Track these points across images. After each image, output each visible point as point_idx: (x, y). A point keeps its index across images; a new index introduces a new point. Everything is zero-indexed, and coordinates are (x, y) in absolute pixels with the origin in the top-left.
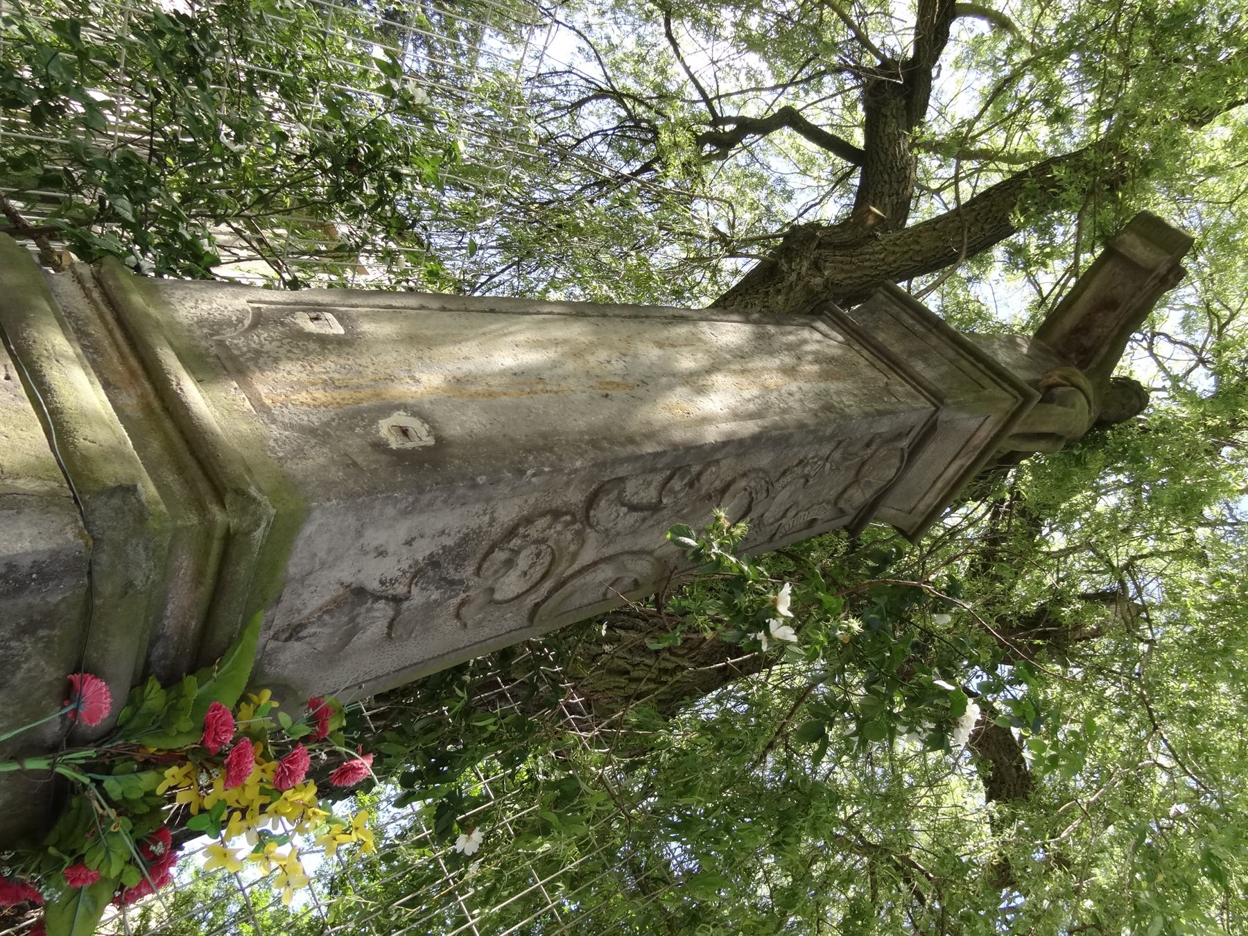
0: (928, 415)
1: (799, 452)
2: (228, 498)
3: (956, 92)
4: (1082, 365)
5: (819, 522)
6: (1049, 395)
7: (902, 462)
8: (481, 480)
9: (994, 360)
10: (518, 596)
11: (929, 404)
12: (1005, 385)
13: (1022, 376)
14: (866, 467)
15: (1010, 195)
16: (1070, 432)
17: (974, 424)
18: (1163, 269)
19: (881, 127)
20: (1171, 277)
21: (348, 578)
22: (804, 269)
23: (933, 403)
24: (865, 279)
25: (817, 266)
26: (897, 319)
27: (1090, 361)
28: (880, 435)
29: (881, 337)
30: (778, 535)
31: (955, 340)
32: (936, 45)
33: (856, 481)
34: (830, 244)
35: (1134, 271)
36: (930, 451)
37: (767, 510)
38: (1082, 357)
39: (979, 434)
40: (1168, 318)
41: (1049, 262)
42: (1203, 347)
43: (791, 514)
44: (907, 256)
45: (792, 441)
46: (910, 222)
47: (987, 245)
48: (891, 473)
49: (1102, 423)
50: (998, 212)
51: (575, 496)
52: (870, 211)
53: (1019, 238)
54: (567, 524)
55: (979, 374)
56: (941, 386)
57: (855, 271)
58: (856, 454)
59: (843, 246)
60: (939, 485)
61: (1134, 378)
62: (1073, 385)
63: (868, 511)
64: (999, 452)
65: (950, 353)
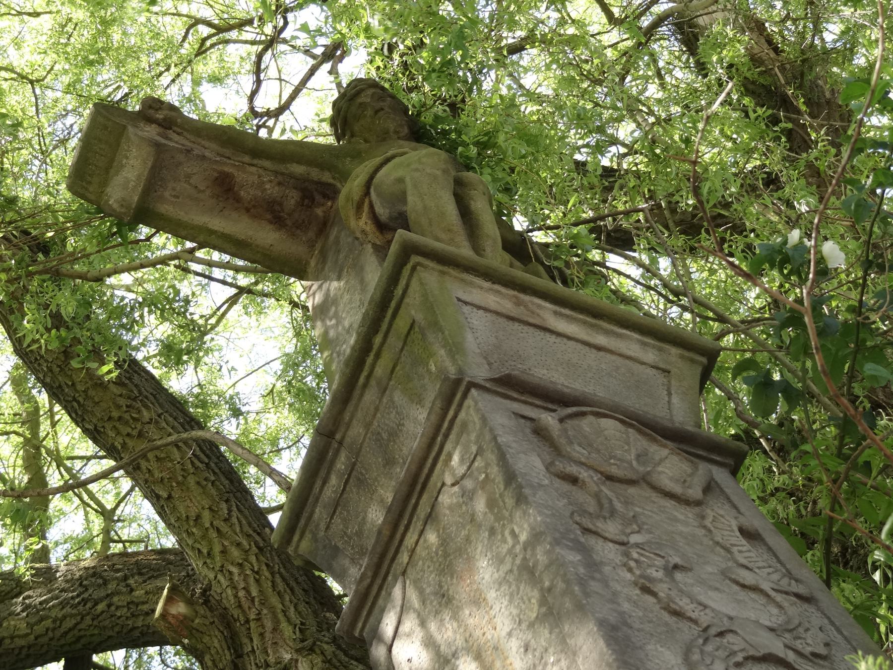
0: (488, 396)
1: (629, 600)
4: (330, 192)
5: (745, 522)
7: (583, 414)
9: (362, 325)
11: (469, 402)
12: (399, 291)
13: (374, 274)
14: (614, 471)
15: (87, 397)
16: (445, 171)
17: (478, 319)
18: (151, 131)
20: (160, 116)
23: (465, 396)
24: (281, 586)
26: (337, 504)
27: (320, 183)
28: (548, 467)
29: (376, 516)
30: (795, 588)
31: (346, 395)
33: (645, 481)
35: (164, 169)
37: (757, 622)
38: (318, 197)
39: (493, 306)
40: (224, 104)
41: (125, 5)
42: (253, 43)
43: (748, 578)
44: (225, 528)
45: (613, 619)
46: (169, 542)
47: (175, 405)
48: (609, 425)
49: (418, 133)
50: (119, 407)
52: (163, 615)
53: (147, 355)
55: (391, 339)
56: (432, 392)
58: (597, 496)
60: (601, 340)
61: (329, 112)
62: (367, 193)
63: (688, 442)
64: (511, 266)
65: (370, 396)
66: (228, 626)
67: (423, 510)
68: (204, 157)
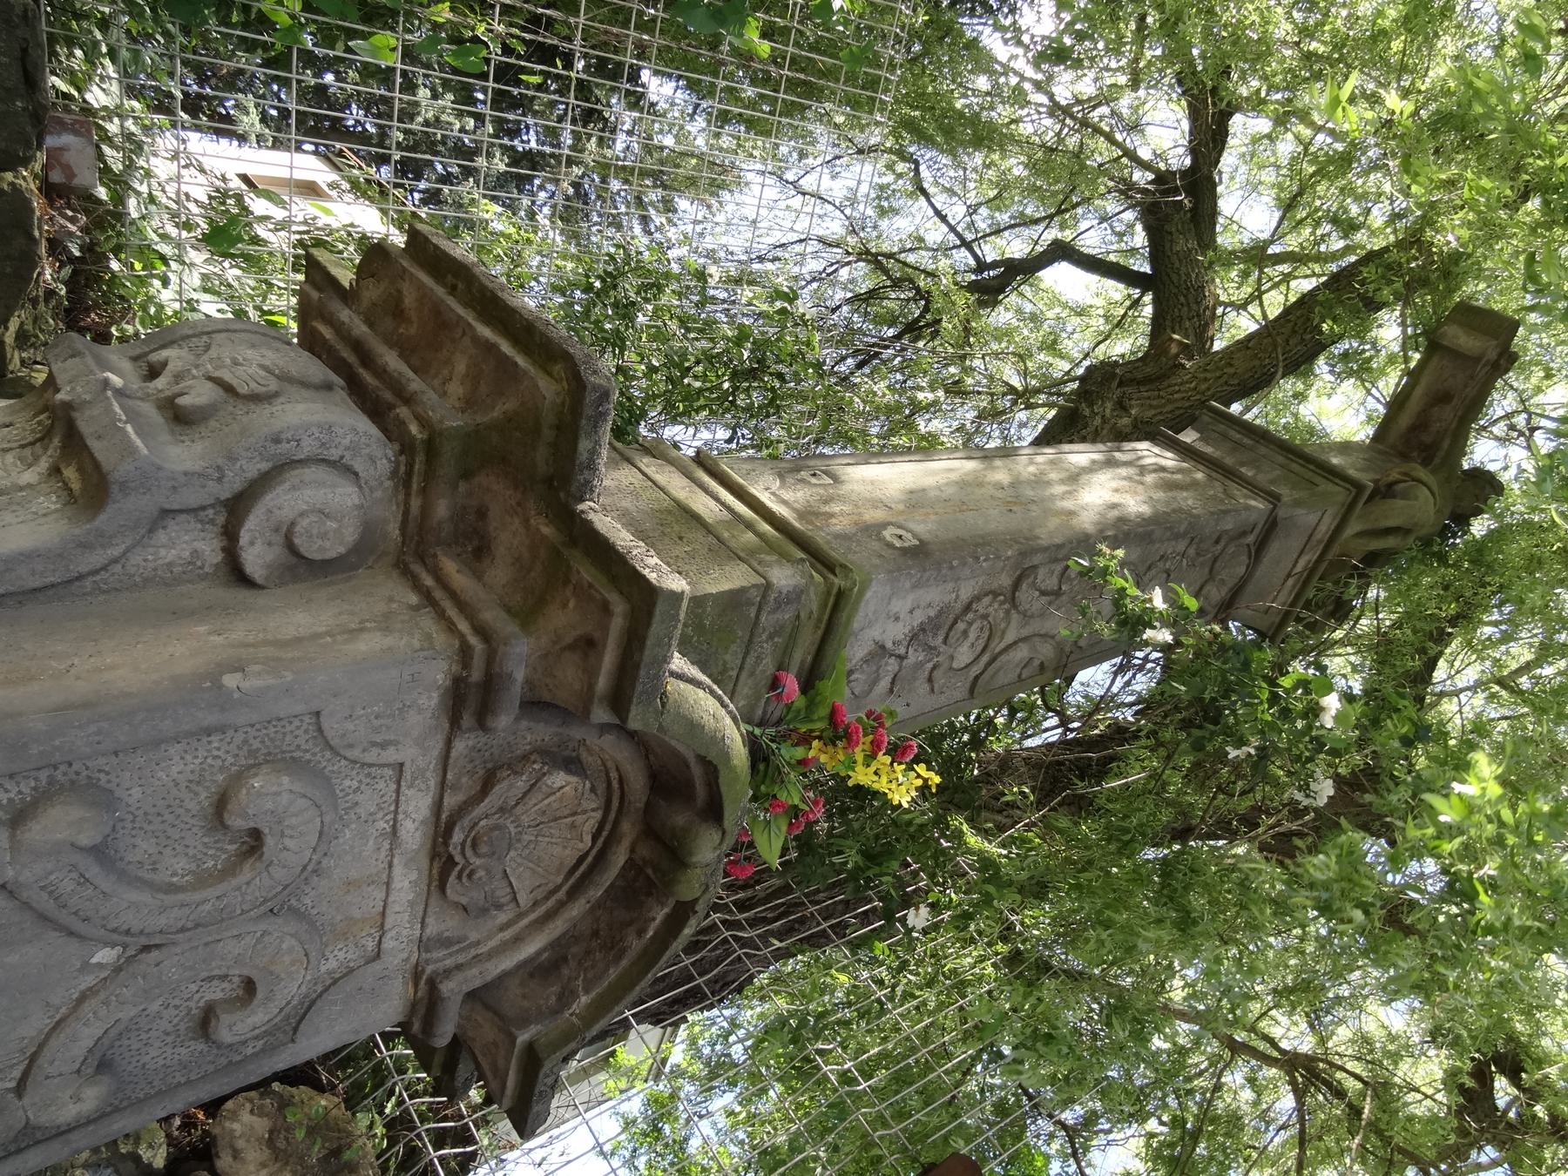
2: (837, 570)
3: (1245, 211)
4: (1426, 462)
6: (1385, 491)
8: (955, 563)
10: (967, 666)
14: (1218, 564)
18: (1492, 355)
19: (1168, 245)
21: (878, 638)
22: (1108, 411)
24: (1178, 413)
25: (1122, 406)
26: (1225, 436)
32: (1215, 147)
34: (1132, 380)
35: (1464, 364)
36: (1274, 549)
46: (1218, 346)
51: (1005, 581)
54: (1002, 603)
57: (1164, 406)
59: (1147, 380)
62: (1413, 480)
65: (1281, 459)
66: (1158, 378)
67: (1214, 474)
68: (1466, 386)
